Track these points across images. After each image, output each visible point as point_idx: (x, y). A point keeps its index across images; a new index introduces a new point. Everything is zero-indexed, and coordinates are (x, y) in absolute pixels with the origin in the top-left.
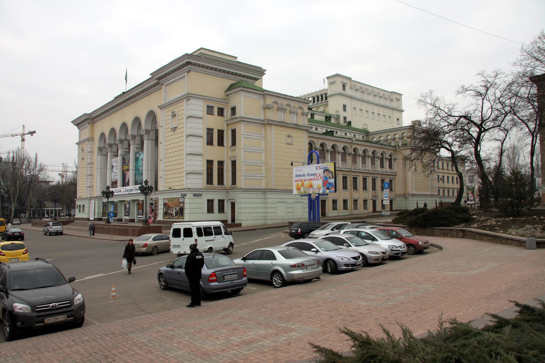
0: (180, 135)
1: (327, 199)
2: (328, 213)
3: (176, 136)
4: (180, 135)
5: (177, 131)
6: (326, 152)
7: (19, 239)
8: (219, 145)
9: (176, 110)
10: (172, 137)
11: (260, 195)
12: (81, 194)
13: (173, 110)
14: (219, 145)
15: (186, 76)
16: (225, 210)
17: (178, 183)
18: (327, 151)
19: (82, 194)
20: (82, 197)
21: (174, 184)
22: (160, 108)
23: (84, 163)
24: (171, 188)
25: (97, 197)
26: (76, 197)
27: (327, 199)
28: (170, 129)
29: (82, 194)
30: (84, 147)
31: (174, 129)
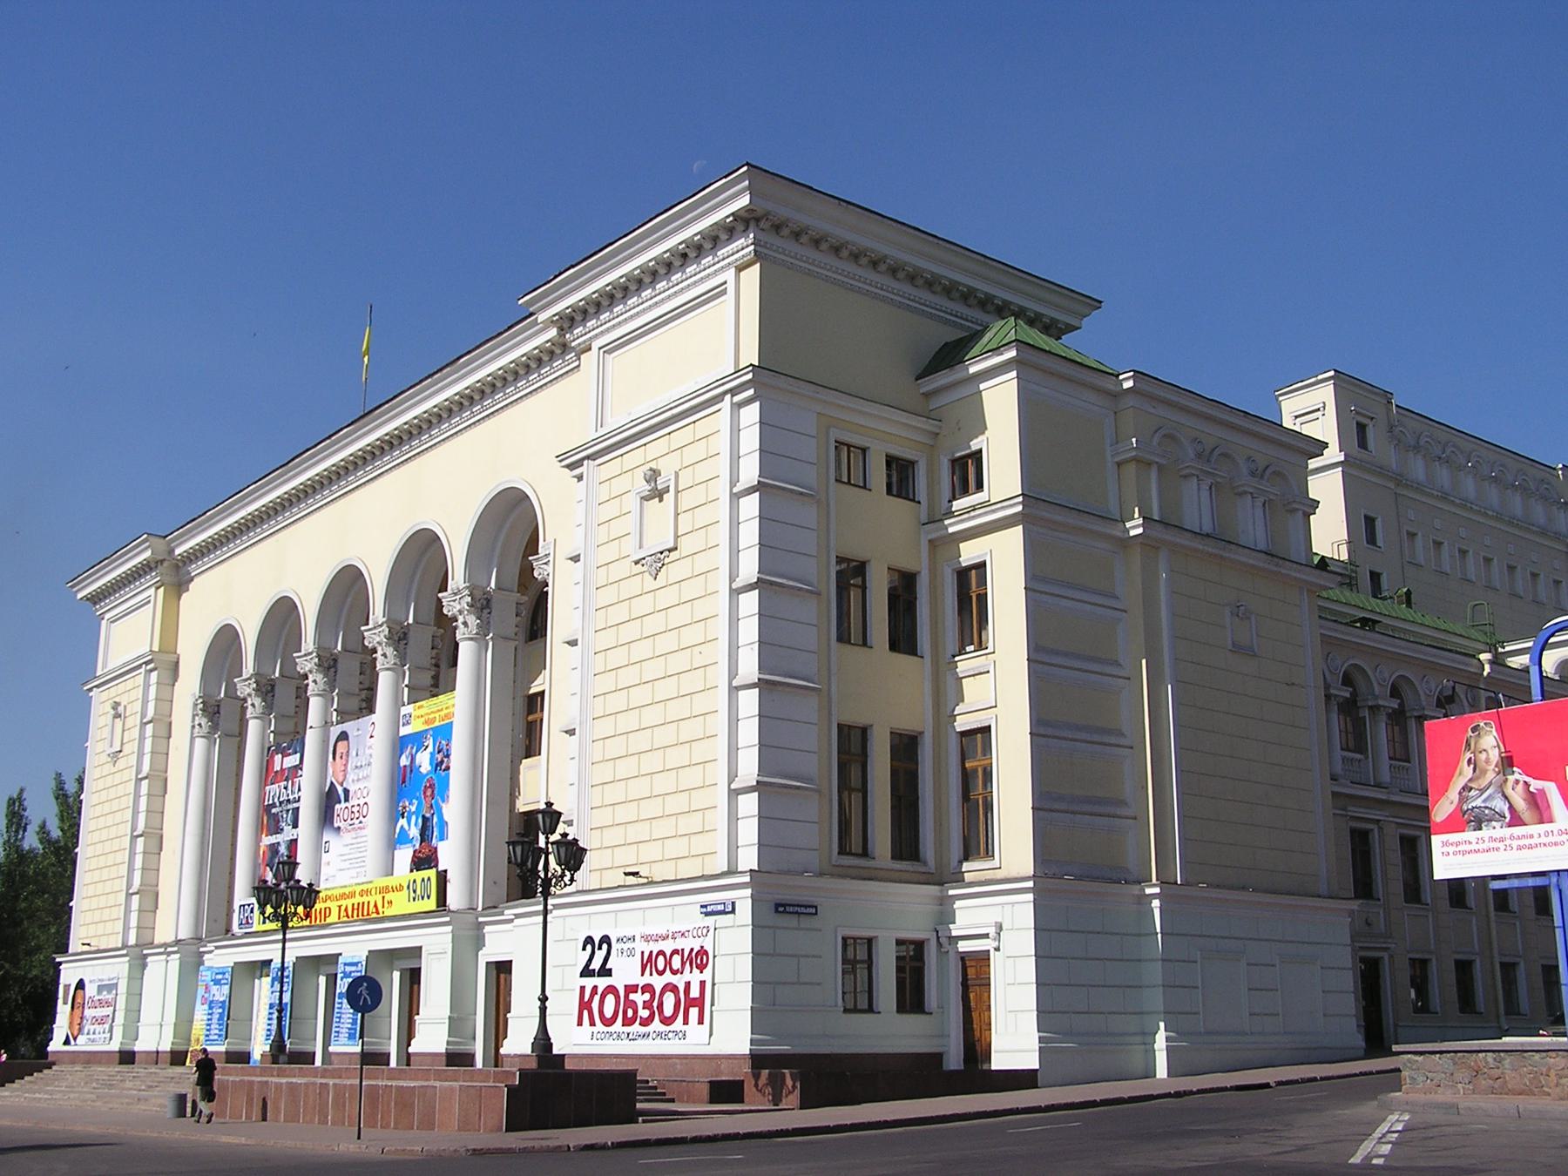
0: (692, 589)
1: (1385, 955)
2: (1396, 1026)
3: (668, 597)
4: (692, 589)
5: (673, 571)
6: (1366, 713)
7: (1541, 1032)
8: (894, 646)
9: (667, 468)
10: (643, 605)
11: (716, 987)
12: (92, 930)
13: (653, 465)
14: (894, 646)
15: (731, 287)
16: (932, 997)
17: (677, 848)
18: (1374, 709)
19: (100, 929)
20: (97, 944)
21: (650, 852)
22: (568, 466)
23: (118, 778)
24: (635, 874)
25: (178, 942)
26: (63, 948)
27: (1385, 955)
28: (628, 562)
29: (100, 929)
30: (124, 700)
31: (658, 561)
